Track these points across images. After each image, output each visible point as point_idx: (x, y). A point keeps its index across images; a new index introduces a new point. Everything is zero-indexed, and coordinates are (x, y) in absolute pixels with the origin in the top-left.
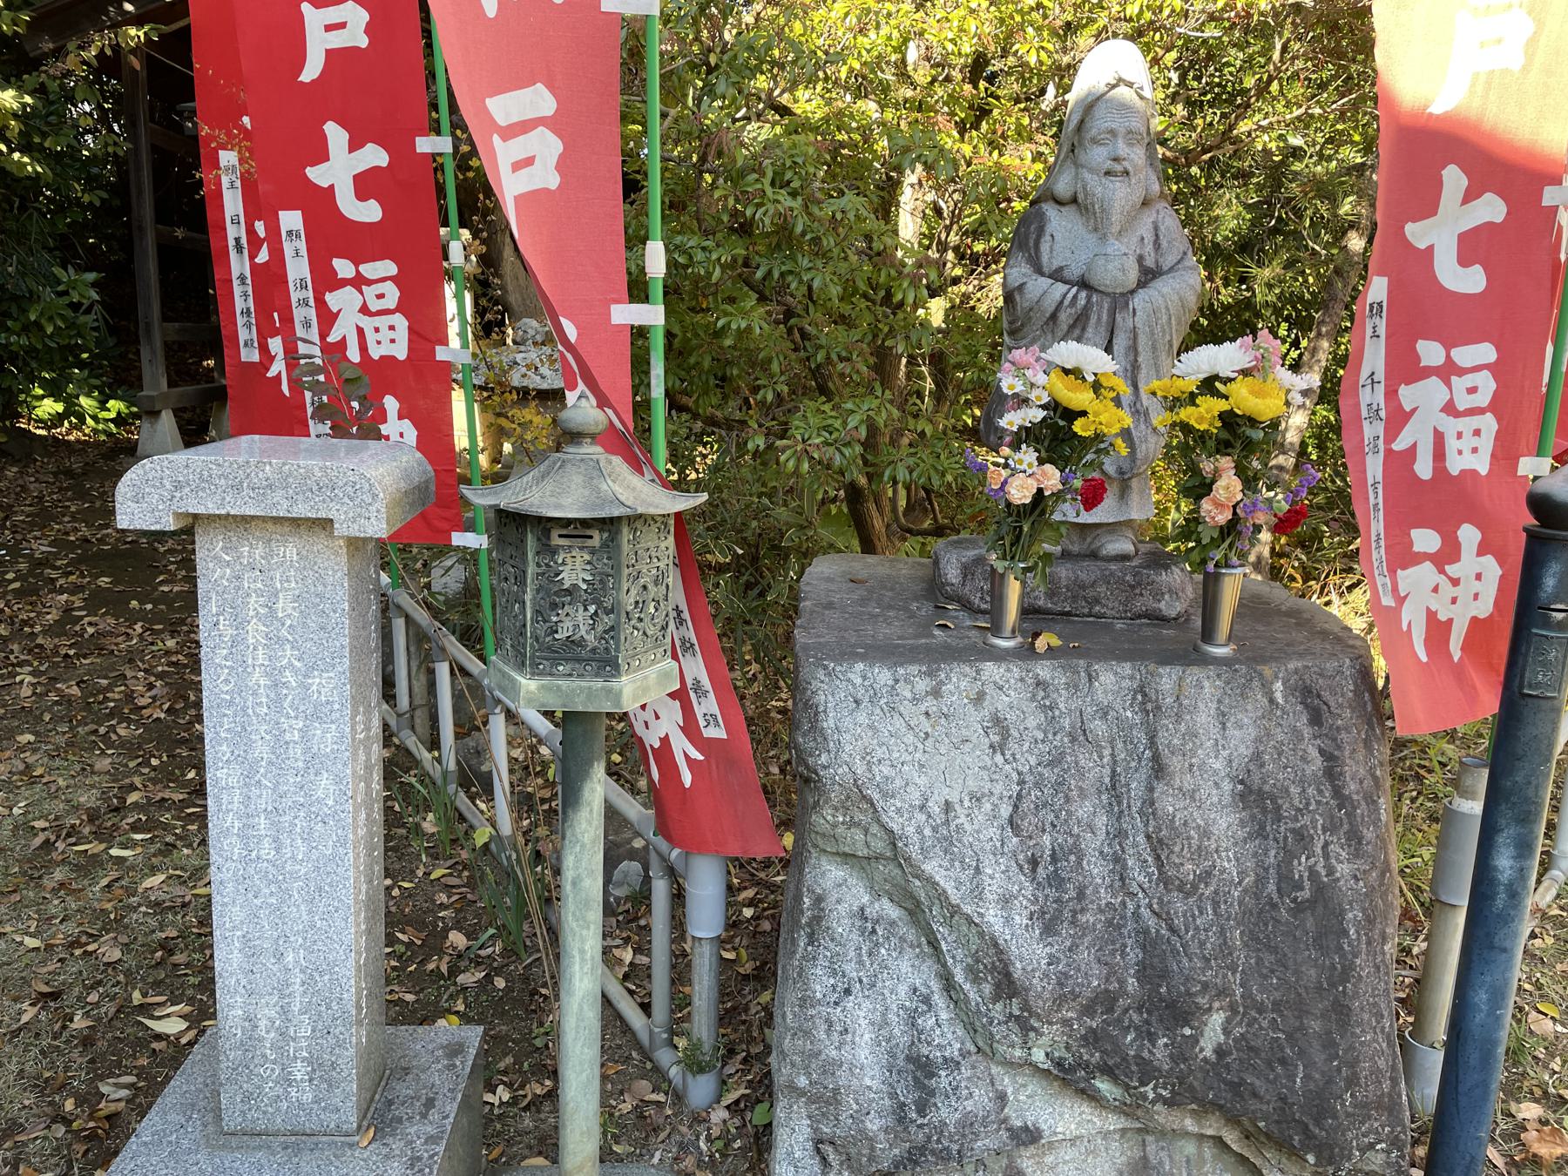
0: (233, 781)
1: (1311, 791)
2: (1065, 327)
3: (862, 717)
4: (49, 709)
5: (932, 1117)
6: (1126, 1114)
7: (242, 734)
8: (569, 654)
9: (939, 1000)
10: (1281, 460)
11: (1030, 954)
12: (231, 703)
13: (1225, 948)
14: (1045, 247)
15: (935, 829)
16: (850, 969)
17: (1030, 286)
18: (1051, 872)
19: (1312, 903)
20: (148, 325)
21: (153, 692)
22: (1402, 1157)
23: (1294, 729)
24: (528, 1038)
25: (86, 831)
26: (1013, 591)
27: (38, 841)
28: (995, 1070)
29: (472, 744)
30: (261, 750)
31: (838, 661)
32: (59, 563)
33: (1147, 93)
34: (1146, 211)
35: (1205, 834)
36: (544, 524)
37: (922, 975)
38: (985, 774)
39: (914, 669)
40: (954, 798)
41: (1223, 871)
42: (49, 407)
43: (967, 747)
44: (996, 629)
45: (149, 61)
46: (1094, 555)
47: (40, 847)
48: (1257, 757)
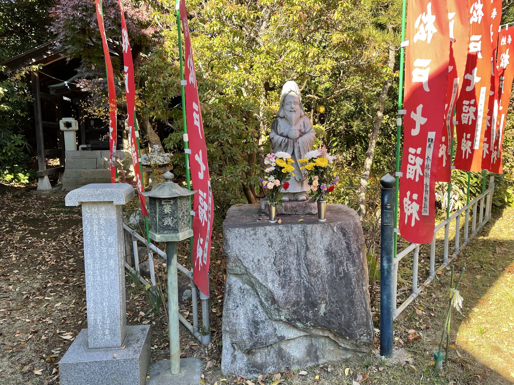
0: (91, 263)
1: (343, 252)
2: (283, 147)
3: (238, 241)
4: (21, 263)
5: (259, 334)
6: (304, 331)
7: (93, 252)
8: (167, 228)
9: (259, 307)
10: (366, 173)
11: (279, 293)
12: (90, 244)
13: (324, 289)
14: (278, 128)
15: (256, 266)
16: (238, 301)
17: (275, 138)
18: (283, 274)
19: (344, 277)
20: (40, 151)
21: (51, 257)
22: (371, 337)
23: (339, 238)
24: (162, 335)
25: (37, 294)
26: (273, 209)
27: (25, 296)
28: (273, 323)
29: (143, 264)
30: (97, 255)
31: (232, 228)
32: (18, 223)
33: (298, 93)
34: (301, 119)
35: (319, 263)
36: (160, 200)
37: (256, 302)
38: (267, 252)
39: (250, 229)
40: (260, 258)
41: (323, 271)
42: (9, 177)
43: (263, 246)
44: (270, 219)
45: (39, 73)
46: (297, 200)
47: (25, 298)
48: (330, 245)
